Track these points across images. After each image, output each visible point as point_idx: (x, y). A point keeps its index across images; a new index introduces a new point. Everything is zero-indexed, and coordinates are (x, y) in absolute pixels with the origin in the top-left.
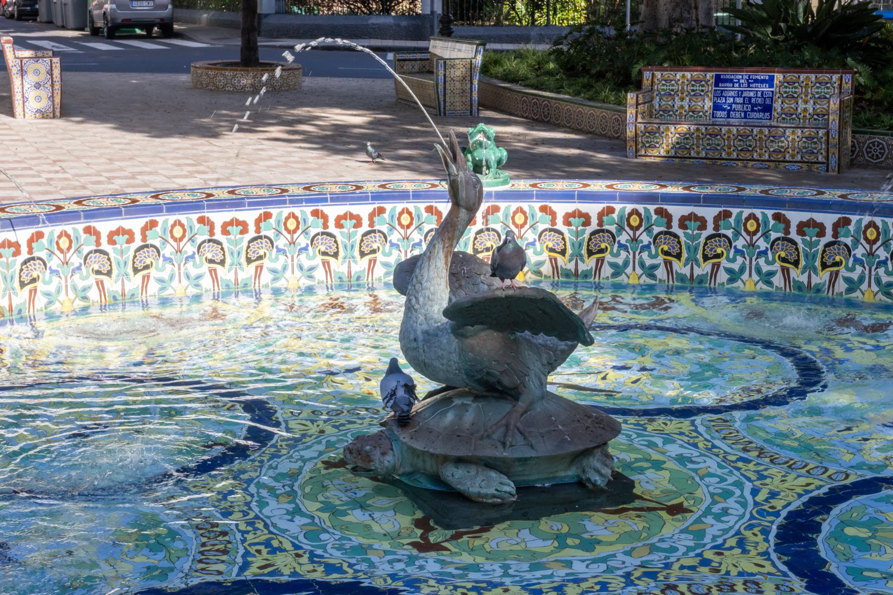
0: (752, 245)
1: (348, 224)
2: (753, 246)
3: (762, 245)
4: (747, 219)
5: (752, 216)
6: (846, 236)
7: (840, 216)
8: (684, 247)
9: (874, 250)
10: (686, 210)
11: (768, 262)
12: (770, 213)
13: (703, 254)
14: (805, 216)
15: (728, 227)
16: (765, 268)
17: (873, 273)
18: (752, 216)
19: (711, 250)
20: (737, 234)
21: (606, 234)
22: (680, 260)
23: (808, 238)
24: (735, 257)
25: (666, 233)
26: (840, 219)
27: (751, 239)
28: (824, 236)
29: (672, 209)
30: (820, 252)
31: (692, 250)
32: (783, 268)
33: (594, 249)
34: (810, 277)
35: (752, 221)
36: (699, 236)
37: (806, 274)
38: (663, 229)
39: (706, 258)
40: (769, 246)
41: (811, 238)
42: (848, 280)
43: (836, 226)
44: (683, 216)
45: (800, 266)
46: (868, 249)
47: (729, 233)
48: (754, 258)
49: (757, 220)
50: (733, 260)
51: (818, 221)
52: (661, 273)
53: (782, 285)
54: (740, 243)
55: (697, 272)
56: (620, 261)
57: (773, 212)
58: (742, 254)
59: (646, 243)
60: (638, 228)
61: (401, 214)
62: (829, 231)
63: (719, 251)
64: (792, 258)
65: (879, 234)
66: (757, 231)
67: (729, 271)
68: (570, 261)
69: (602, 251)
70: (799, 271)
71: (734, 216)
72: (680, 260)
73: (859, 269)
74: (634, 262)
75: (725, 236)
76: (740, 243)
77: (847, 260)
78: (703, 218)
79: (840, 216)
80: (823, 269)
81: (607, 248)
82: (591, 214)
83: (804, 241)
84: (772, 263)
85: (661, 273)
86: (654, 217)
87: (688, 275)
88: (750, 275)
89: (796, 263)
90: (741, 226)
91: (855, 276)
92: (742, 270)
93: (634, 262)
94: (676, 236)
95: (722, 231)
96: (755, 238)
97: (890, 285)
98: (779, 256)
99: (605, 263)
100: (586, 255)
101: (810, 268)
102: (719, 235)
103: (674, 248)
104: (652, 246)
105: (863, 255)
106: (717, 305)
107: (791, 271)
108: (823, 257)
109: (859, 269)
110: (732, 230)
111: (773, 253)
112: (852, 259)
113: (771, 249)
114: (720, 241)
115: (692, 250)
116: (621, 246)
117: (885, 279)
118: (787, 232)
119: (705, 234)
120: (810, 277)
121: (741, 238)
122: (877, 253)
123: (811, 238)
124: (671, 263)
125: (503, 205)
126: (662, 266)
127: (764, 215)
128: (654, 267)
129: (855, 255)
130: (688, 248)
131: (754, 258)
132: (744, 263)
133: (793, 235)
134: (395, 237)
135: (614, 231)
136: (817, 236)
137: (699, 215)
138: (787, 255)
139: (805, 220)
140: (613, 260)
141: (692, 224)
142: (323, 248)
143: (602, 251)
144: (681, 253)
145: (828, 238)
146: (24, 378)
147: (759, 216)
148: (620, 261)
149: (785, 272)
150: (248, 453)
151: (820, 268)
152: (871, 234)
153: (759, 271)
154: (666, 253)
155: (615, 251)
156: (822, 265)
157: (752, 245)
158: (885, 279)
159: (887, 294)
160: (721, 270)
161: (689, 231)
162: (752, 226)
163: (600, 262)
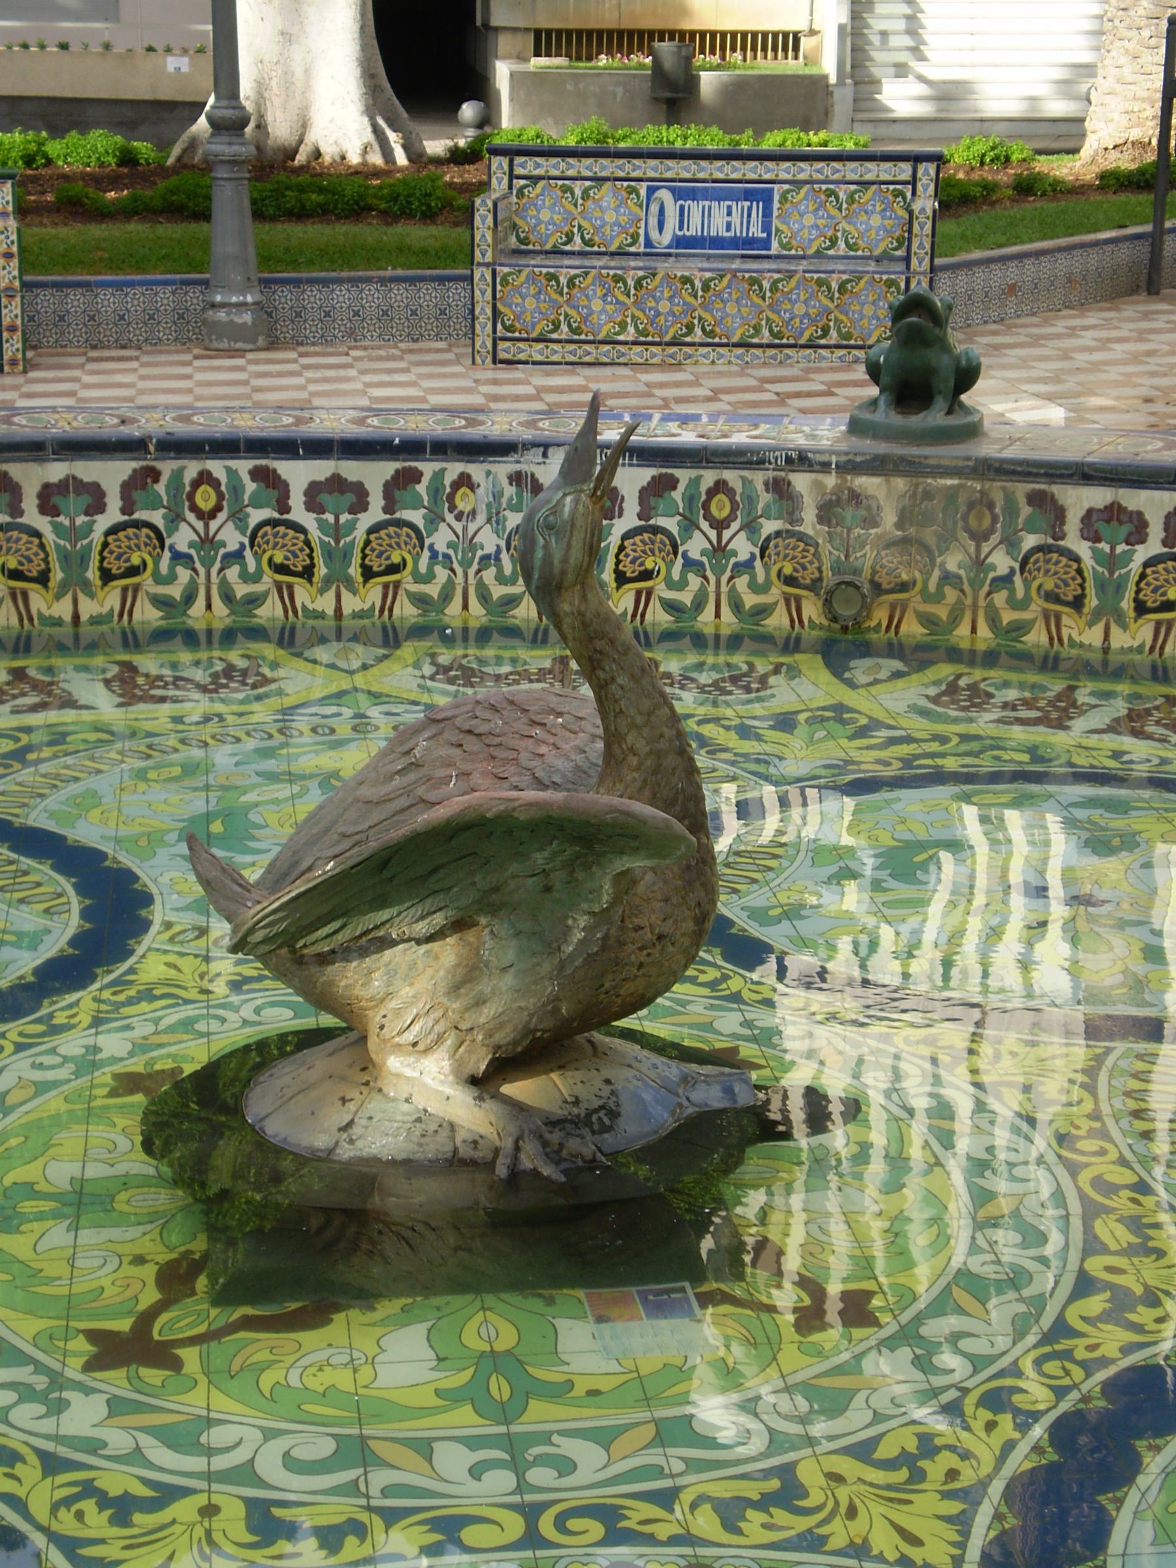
0: (719, 550)
3: (232, 538)
7: (135, 465)
8: (1090, 585)
9: (211, 533)
10: (56, 471)
11: (754, 587)
21: (145, 531)
22: (310, 581)
23: (330, 518)
26: (653, 478)
28: (365, 509)
29: (287, 469)
32: (1046, 615)
34: (75, 602)
46: (972, 550)
48: (724, 579)
49: (215, 483)
50: (682, 585)
51: (87, 479)
54: (696, 546)
55: (351, 604)
65: (220, 496)
66: (218, 508)
72: (310, 581)
76: (696, 546)
77: (157, 559)
79: (135, 465)
80: (105, 584)
81: (404, 561)
82: (104, 486)
86: (250, 487)
91: (175, 591)
94: (299, 529)
95: (662, 522)
98: (270, 560)
102: (138, 525)
104: (758, 563)
105: (191, 545)
107: (1065, 620)
109: (184, 575)
113: (252, 545)
118: (284, 508)
119: (366, 520)
121: (697, 533)
122: (989, 560)
127: (231, 473)
129: (943, 564)
131: (724, 579)
132: (959, 602)
135: (675, 530)
136: (87, 514)
137: (86, 479)
139: (321, 477)
143: (647, 575)
147: (737, 485)
148: (175, 591)
150: (797, 1278)
152: (205, 498)
160: (402, 599)
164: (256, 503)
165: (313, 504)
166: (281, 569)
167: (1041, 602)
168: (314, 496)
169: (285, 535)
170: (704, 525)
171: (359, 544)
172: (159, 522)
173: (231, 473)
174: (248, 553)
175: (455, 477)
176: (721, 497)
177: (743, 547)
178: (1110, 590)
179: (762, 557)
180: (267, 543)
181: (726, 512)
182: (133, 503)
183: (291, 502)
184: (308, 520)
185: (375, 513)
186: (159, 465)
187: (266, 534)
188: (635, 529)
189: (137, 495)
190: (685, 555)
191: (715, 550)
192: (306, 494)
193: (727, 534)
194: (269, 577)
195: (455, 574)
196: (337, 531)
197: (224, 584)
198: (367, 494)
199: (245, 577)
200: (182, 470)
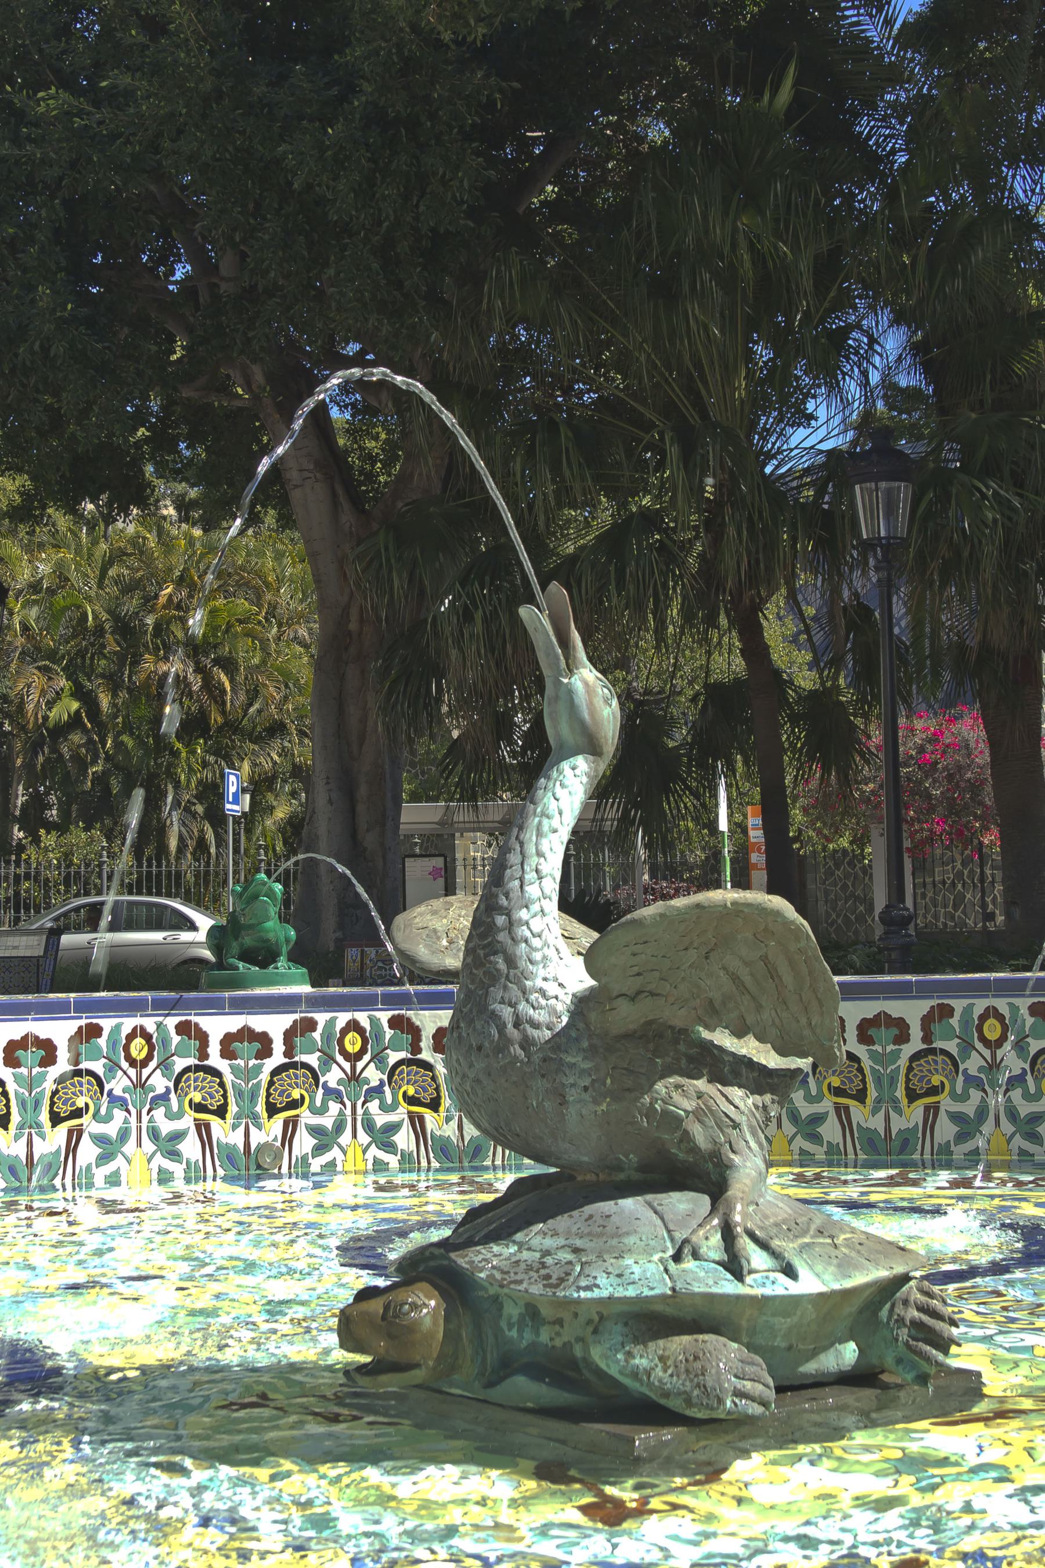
0: (354, 1078)
1: (30, 1056)
2: (143, 1086)
3: (160, 1083)
4: (983, 1018)
5: (354, 1026)
6: (947, 1038)
8: (869, 1079)
9: (358, 1071)
11: (384, 1108)
12: (384, 1017)
13: (907, 1088)
14: (870, 1009)
15: (950, 1035)
16: (381, 1120)
17: (360, 1111)
18: (354, 1026)
19: (921, 1080)
20: (113, 1066)
22: (223, 1118)
24: (966, 1091)
25: (198, 1068)
26: (295, 1022)
27: (353, 1068)
28: (907, 1040)
30: (903, 1071)
31: (886, 1081)
33: (920, 1087)
34: (887, 1119)
35: (991, 1021)
36: (258, 1069)
37: (881, 1114)
38: (192, 1061)
39: (912, 1096)
40: (171, 1085)
41: (884, 1048)
42: (957, 1118)
43: (927, 1021)
44: (864, 1021)
45: (868, 1101)
47: (952, 1046)
49: (360, 1030)
51: (895, 1015)
52: (404, 1139)
53: (413, 1147)
54: (333, 1077)
55: (898, 1124)
56: (327, 1122)
57: (390, 1014)
58: (979, 1085)
59: (160, 1090)
60: (359, 1056)
61: (131, 1037)
62: (916, 1032)
63: (296, 1094)
64: (853, 1088)
65: (365, 1041)
66: (363, 1051)
67: (957, 1118)
68: (17, 1138)
69: (934, 1091)
70: (867, 1111)
71: (320, 1028)
72: (223, 1118)
73: (334, 1107)
74: (354, 1120)
75: (944, 1052)
76: (333, 1077)
78: (902, 1019)
81: (87, 1105)
82: (272, 1035)
83: (873, 1055)
84: (392, 1108)
85: (831, 1130)
86: (389, 1033)
87: (241, 1146)
88: (355, 1135)
89: (861, 1096)
90: (335, 1040)
92: (339, 1127)
93: (354, 1120)
94: (427, 1066)
95: (939, 1044)
96: (146, 1072)
97: (1035, 1118)
98: (405, 1093)
99: (942, 1115)
100: (905, 1101)
101: (887, 1102)
103: (851, 1081)
104: (387, 1088)
105: (981, 1069)
106: (23, 1200)
108: (908, 1080)
109: (334, 1107)
110: (318, 1054)
111: (393, 1089)
112: (961, 1078)
114: (936, 1062)
115: (886, 1081)
116: (329, 1092)
117: (1025, 1109)
119: (908, 1050)
120: (887, 1119)
121: (974, 1053)
123: (884, 1048)
124: (208, 1127)
125: (321, 1018)
126: (832, 1118)
127: (373, 1021)
128: (818, 1119)
129: (325, 1083)
130: (239, 1094)
132: (341, 1113)
133: (215, 1060)
134: (118, 1085)
135: (954, 1051)
136: (40, 1066)
138: (204, 1098)
139: (234, 1030)
140: (97, 1128)
141: (243, 1047)
142: (197, 1097)
144: (439, 1097)
145: (916, 1044)
146: (918, 1481)
147: (365, 1023)
148: (327, 1122)
149: (842, 1113)
151: (905, 1101)
153: (369, 1126)
154: (411, 1101)
155: (318, 1103)
156: (907, 1096)
157: (354, 1078)
158: (1025, 1109)
159: (1033, 1137)
160: (942, 1116)
161: (878, 1048)
162: (992, 1028)
163: (290, 1126)
164: (180, 1053)
165: (227, 1053)
166: (200, 1108)
167: (192, 1113)
168: (228, 1041)
169: (417, 1073)
170: (340, 1058)
171: (264, 1085)
172: (100, 1071)
173: (373, 1021)
174: (1029, 1078)
175: (343, 1025)
176: (991, 1021)
177: (373, 1075)
178: (29, 1106)
179: (1032, 1072)
180: (189, 1087)
181: (358, 1047)
182: (79, 1055)
183: (209, 1050)
184: (222, 1065)
185: (63, 1065)
186: (101, 1022)
187: (402, 1072)
188: (920, 1052)
189: (936, 1028)
190: (325, 1085)
191: (991, 1067)
192: (222, 1042)
193: (360, 1065)
194: (403, 1109)
195: (130, 1113)
196: (31, 1083)
197: (366, 1113)
198: (271, 1041)
199: (170, 1116)
200: (333, 1020)
